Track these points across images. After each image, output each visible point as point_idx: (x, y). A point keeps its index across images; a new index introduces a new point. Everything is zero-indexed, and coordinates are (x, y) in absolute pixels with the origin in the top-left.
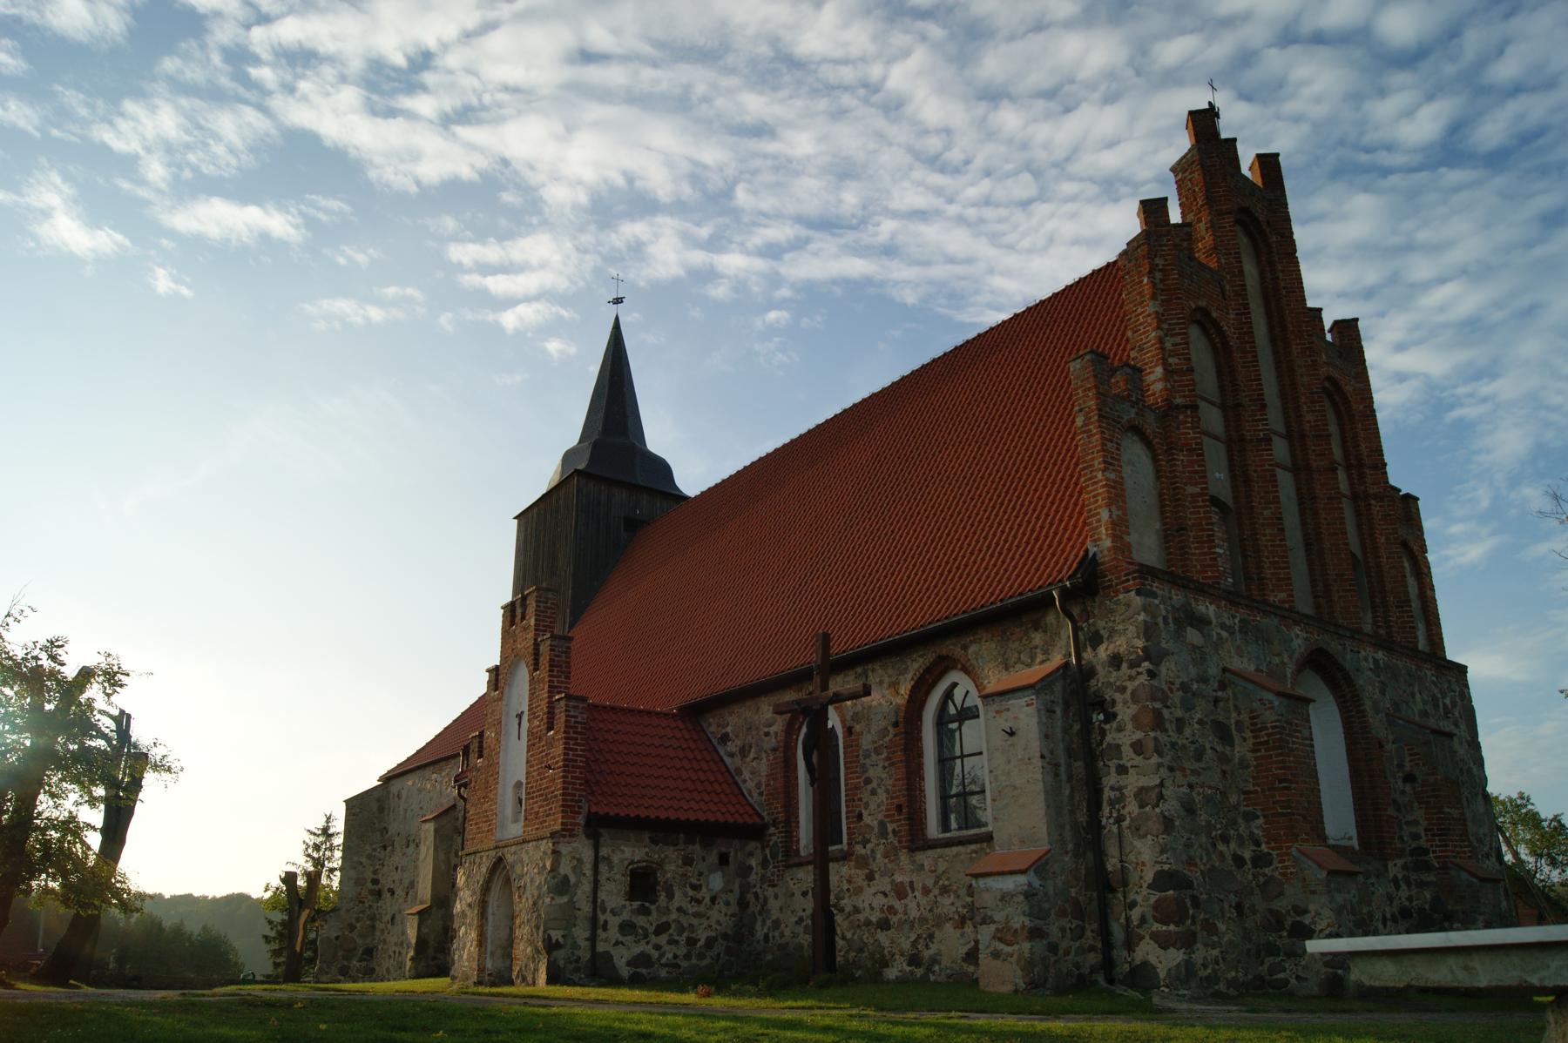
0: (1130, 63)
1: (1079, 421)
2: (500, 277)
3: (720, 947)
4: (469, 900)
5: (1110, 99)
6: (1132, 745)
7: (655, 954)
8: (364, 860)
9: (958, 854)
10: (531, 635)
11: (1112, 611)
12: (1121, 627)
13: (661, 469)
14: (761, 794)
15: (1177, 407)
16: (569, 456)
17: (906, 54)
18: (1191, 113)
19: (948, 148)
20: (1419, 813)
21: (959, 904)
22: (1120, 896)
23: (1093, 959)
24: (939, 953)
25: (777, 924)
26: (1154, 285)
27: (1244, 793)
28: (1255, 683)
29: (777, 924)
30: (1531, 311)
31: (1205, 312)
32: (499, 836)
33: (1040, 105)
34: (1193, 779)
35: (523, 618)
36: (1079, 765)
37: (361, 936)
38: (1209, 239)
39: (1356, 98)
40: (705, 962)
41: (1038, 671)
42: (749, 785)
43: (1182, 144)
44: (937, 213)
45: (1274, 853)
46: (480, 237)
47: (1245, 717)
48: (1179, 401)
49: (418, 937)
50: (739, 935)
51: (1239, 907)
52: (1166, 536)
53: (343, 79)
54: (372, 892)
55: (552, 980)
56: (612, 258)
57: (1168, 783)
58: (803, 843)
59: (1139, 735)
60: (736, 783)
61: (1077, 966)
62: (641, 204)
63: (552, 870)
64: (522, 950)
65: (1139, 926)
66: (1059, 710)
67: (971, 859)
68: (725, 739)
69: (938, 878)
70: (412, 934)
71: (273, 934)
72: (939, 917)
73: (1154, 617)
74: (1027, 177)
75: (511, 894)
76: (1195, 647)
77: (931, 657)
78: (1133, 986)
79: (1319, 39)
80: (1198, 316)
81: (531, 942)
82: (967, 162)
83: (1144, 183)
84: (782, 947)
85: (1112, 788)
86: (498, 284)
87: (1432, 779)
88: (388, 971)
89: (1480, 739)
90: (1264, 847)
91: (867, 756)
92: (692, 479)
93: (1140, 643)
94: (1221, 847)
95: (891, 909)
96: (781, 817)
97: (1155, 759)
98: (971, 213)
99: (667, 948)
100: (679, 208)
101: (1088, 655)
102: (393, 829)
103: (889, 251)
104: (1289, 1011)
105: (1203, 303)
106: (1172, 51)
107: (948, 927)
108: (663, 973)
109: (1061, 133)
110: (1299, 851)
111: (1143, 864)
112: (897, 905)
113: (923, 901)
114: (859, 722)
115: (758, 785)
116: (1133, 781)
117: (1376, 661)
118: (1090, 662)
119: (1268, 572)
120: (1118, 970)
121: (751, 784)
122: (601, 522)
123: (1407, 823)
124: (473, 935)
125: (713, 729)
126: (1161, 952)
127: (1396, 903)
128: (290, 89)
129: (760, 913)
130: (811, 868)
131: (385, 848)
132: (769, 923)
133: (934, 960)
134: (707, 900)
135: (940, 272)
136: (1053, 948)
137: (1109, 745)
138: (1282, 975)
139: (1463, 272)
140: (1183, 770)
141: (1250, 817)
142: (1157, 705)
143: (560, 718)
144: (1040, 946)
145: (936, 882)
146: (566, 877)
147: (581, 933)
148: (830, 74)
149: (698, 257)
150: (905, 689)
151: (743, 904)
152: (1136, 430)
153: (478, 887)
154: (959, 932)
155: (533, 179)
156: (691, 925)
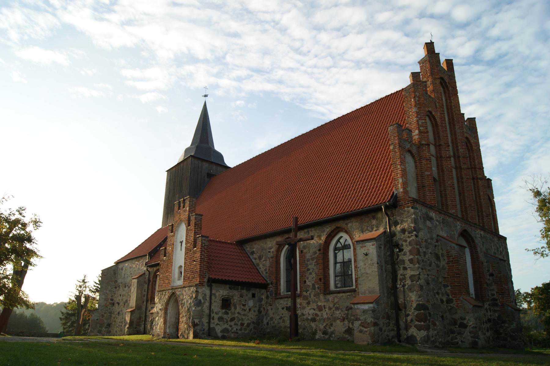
1: (391, 147)
3: (252, 326)
4: (160, 307)
5: (360, 32)
6: (409, 260)
7: (230, 328)
8: (108, 292)
9: (342, 296)
10: (187, 213)
11: (402, 214)
12: (405, 219)
13: (220, 156)
14: (266, 273)
15: (423, 144)
16: (187, 151)
17: (289, 11)
19: (302, 46)
22: (403, 312)
23: (393, 333)
24: (335, 330)
25: (272, 319)
26: (416, 102)
27: (445, 278)
28: (446, 239)
30: (499, 116)
32: (172, 285)
33: (335, 33)
35: (184, 207)
40: (246, 332)
41: (375, 234)
42: (262, 269)
43: (422, 53)
44: (298, 69)
45: (454, 299)
47: (445, 252)
48: (423, 142)
49: (130, 320)
50: (258, 323)
51: (442, 317)
52: (418, 189)
53: (85, 6)
54: (110, 303)
55: (195, 337)
57: (421, 274)
58: (282, 291)
59: (411, 257)
62: (193, 60)
64: (183, 326)
65: (410, 322)
66: (383, 247)
67: (347, 298)
68: (253, 253)
69: (335, 304)
70: (128, 319)
71: (63, 317)
72: (335, 318)
75: (178, 306)
78: (407, 343)
80: (428, 113)
81: (186, 323)
82: (309, 52)
85: (401, 275)
86: (140, 85)
87: (499, 275)
88: (116, 331)
89: (510, 262)
90: (450, 297)
91: (308, 260)
93: (413, 225)
94: (437, 296)
95: (316, 315)
97: (417, 265)
98: (309, 70)
100: (206, 61)
101: (393, 228)
103: (280, 82)
104: (464, 353)
105: (430, 109)
106: (382, 17)
107: (338, 321)
108: (232, 335)
109: (340, 44)
111: (412, 301)
112: (319, 313)
113: (329, 312)
114: (305, 249)
115: (265, 270)
116: (409, 273)
117: (481, 235)
118: (394, 231)
119: (449, 203)
121: (263, 269)
122: (198, 175)
123: (490, 290)
124: (162, 320)
125: (248, 249)
126: (418, 332)
127: (487, 317)
128: (65, 9)
129: (265, 315)
131: (116, 288)
132: (269, 318)
133: (333, 333)
134: (248, 310)
137: (400, 260)
138: (456, 340)
139: (478, 101)
140: (426, 269)
141: (446, 286)
142: (418, 247)
143: (199, 243)
145: (334, 306)
146: (200, 300)
147: (205, 320)
149: (213, 80)
150: (323, 238)
151: (260, 312)
152: (410, 151)
153: (164, 303)
156: (242, 319)
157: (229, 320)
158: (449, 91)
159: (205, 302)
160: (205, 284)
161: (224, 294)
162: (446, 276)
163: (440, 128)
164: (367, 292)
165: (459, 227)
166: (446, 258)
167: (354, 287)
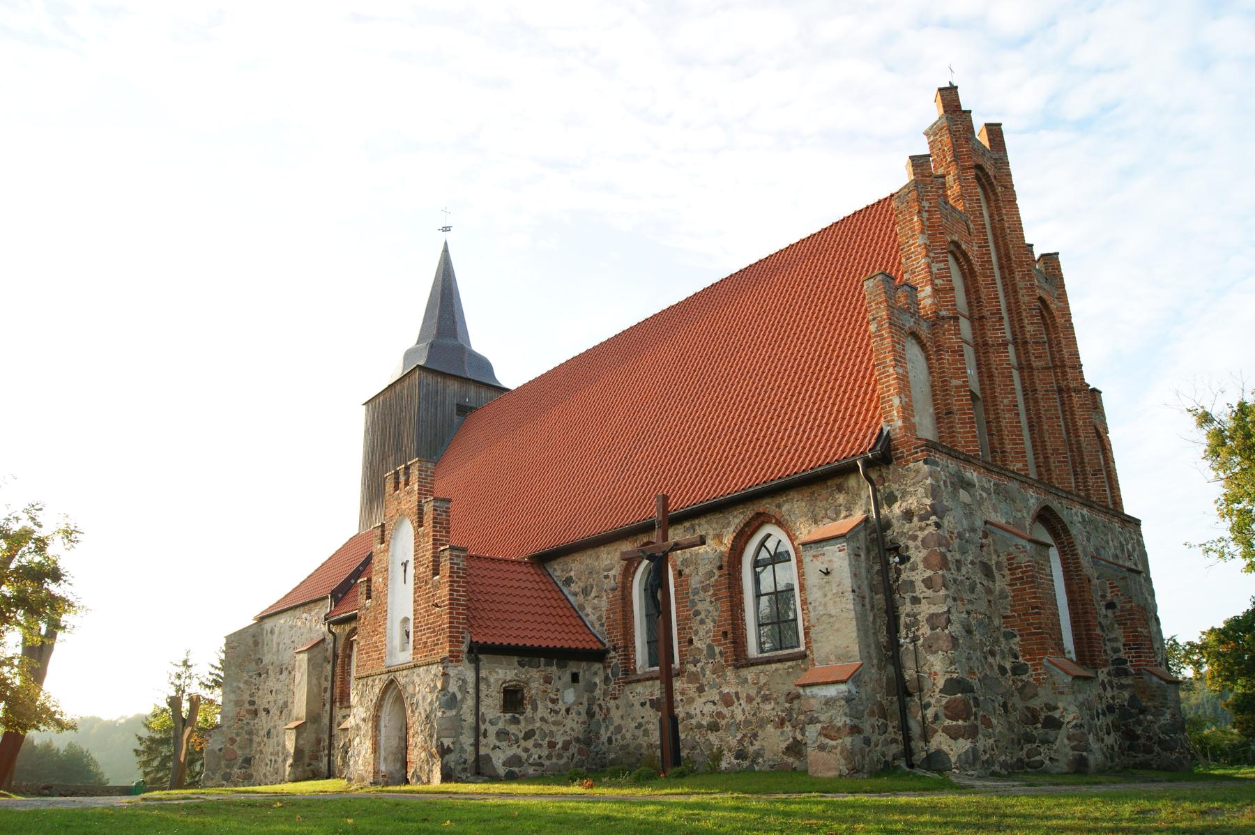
1: (872, 328)
3: (574, 749)
4: (363, 715)
6: (923, 581)
7: (524, 755)
8: (241, 685)
10: (415, 497)
11: (904, 476)
12: (911, 489)
14: (602, 625)
15: (943, 318)
16: (409, 355)
18: (940, 90)
20: (1118, 632)
21: (778, 709)
23: (895, 749)
24: (763, 748)
25: (619, 729)
27: (1004, 617)
29: (619, 729)
32: (388, 662)
35: (407, 484)
36: (880, 597)
37: (240, 748)
40: (562, 761)
41: (844, 525)
42: (591, 616)
47: (1003, 559)
48: (944, 313)
49: (296, 747)
50: (587, 740)
51: (1005, 706)
52: (938, 419)
54: (249, 711)
55: (447, 777)
57: (953, 610)
58: (639, 664)
59: (929, 573)
63: (442, 690)
64: (416, 756)
65: (933, 723)
67: (788, 673)
68: (568, 581)
69: (760, 689)
70: (290, 746)
71: (141, 748)
72: (762, 719)
73: (937, 481)
76: (966, 506)
80: (952, 248)
84: (623, 748)
85: (908, 615)
87: (1128, 606)
88: (265, 775)
91: (696, 593)
93: (928, 501)
94: (991, 660)
95: (719, 714)
96: (621, 643)
97: (943, 592)
101: (885, 511)
104: (1057, 784)
105: (956, 238)
108: (531, 771)
111: (936, 674)
112: (725, 711)
115: (600, 618)
116: (925, 609)
117: (1082, 516)
118: (886, 516)
119: (1008, 447)
120: (915, 757)
121: (593, 618)
122: (439, 405)
125: (558, 573)
129: (604, 720)
130: (658, 682)
131: (260, 675)
132: (612, 728)
133: (758, 754)
134: (563, 711)
136: (867, 741)
137: (904, 581)
140: (962, 600)
142: (943, 550)
144: (858, 739)
145: (758, 693)
146: (454, 694)
147: (467, 740)
150: (728, 539)
151: (591, 714)
152: (914, 335)
153: (371, 705)
156: (551, 732)
158: (995, 194)
159: (464, 699)
160: (464, 656)
162: (1009, 613)
163: (980, 279)
165: (1032, 501)
166: (1006, 572)
167: (802, 648)
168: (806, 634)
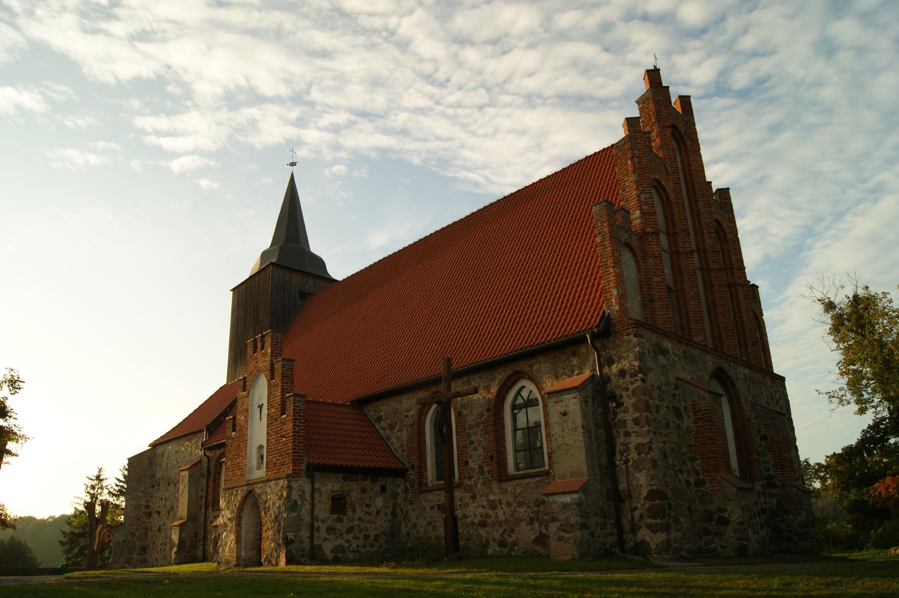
0: (541, 26)
2: (168, 139)
4: (229, 516)
5: (532, 46)
6: (633, 420)
7: (346, 545)
8: (140, 494)
10: (268, 358)
13: (319, 263)
14: (403, 451)
16: (264, 255)
17: (411, 12)
22: (627, 504)
25: (415, 526)
29: (415, 526)
30: (761, 181)
31: (658, 181)
32: (248, 477)
33: (489, 48)
34: (665, 439)
35: (262, 348)
36: (602, 432)
38: (658, 141)
39: (669, 53)
40: (374, 549)
41: (577, 379)
42: (395, 444)
43: (642, 87)
44: (431, 109)
46: (156, 112)
47: (689, 404)
48: (649, 230)
49: (179, 539)
51: (689, 509)
52: (644, 305)
54: (144, 513)
55: (289, 561)
56: (238, 130)
58: (430, 479)
59: (637, 415)
60: (388, 445)
61: (604, 544)
62: (257, 99)
64: (268, 545)
65: (639, 521)
66: (590, 402)
67: (537, 486)
68: (379, 419)
70: (175, 538)
71: (65, 540)
74: (482, 91)
75: (259, 512)
77: (510, 371)
79: (645, 18)
80: (655, 183)
82: (448, 80)
83: (549, 98)
85: (622, 444)
86: (168, 143)
88: (156, 560)
91: (471, 428)
92: (340, 268)
93: (637, 364)
94: (680, 476)
95: (487, 515)
97: (646, 428)
98: (450, 111)
99: (353, 541)
101: (606, 370)
102: (159, 475)
103: (404, 132)
105: (657, 177)
106: (566, 20)
107: (523, 524)
108: (351, 556)
109: (500, 67)
110: (721, 478)
111: (641, 486)
112: (491, 512)
113: (507, 510)
115: (401, 446)
116: (634, 440)
118: (607, 374)
121: (397, 446)
123: (763, 462)
124: (233, 537)
125: (372, 413)
128: (30, 14)
131: (153, 487)
132: (410, 525)
133: (515, 544)
134: (374, 513)
135: (433, 145)
137: (619, 420)
138: (713, 546)
140: (660, 434)
141: (693, 459)
142: (647, 398)
143: (290, 407)
145: (515, 500)
146: (296, 501)
147: (305, 534)
148: (365, 22)
149: (291, 131)
150: (494, 390)
151: (394, 515)
152: (628, 245)
153: (235, 509)
154: (529, 527)
155: (187, 78)
156: (366, 528)
157: (344, 531)
158: (686, 146)
159: (303, 504)
161: (335, 489)
162: (693, 443)
163: (674, 206)
164: (568, 475)
166: (691, 414)
167: (547, 468)
168: (550, 458)
